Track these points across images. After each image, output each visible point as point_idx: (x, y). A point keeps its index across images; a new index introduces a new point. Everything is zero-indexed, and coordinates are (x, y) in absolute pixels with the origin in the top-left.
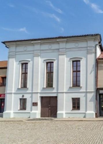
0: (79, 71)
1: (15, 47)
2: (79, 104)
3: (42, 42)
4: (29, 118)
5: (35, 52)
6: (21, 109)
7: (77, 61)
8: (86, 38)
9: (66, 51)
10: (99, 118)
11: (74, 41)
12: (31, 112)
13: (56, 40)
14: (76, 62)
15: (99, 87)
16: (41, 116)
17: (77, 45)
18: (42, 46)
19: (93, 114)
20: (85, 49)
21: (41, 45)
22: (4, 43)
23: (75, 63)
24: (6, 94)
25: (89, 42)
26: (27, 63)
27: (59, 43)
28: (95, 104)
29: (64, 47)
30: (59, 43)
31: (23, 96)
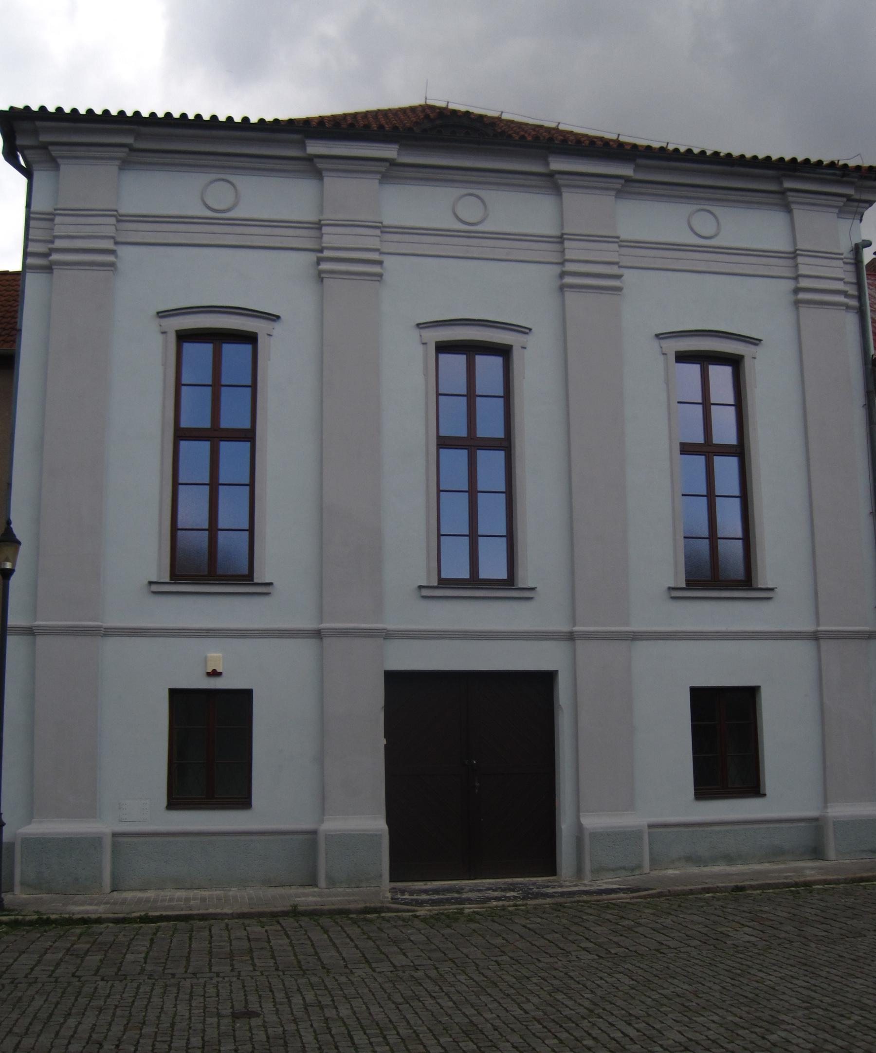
0: (444, 443)
14: (206, 349)
25: (67, 169)
27: (319, 175)
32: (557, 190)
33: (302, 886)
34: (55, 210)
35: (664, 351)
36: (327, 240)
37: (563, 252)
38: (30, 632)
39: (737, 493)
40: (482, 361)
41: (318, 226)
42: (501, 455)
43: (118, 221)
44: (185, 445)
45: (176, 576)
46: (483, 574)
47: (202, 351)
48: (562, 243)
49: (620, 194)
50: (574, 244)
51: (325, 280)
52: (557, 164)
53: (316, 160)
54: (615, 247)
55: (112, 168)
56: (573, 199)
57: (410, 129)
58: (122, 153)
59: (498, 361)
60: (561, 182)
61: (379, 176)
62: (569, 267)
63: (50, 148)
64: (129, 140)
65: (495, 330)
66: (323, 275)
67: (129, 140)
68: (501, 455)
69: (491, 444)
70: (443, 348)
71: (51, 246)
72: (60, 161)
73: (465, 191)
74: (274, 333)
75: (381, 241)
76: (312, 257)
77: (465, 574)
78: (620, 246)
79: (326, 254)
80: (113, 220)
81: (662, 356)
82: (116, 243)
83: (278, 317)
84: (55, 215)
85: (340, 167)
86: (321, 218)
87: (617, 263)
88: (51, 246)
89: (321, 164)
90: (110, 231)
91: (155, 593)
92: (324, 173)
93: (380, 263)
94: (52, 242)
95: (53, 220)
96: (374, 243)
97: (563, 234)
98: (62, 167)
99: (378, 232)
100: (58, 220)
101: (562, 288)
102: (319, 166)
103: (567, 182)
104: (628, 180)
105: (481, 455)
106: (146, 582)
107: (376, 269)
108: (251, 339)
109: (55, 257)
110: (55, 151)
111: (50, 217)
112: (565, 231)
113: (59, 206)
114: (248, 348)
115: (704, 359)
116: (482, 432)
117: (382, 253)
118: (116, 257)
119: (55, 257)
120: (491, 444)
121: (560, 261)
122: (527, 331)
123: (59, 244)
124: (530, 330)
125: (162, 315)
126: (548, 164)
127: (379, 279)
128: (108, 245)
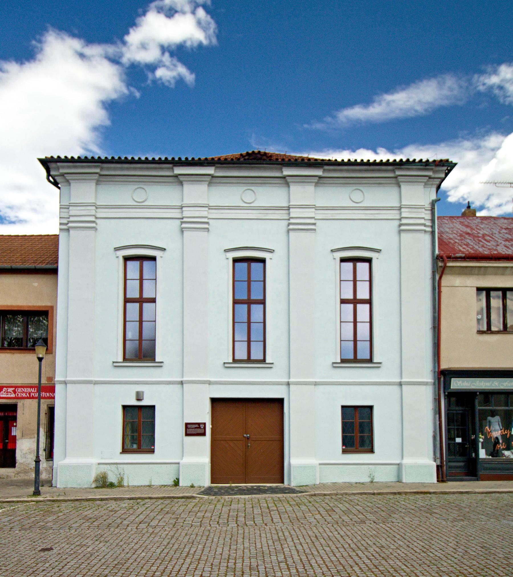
0: (153, 300)
1: (94, 184)
2: (346, 427)
3: (326, 175)
4: (176, 483)
5: (72, 213)
6: (125, 451)
7: (141, 258)
8: (398, 173)
9: (96, 218)
10: (450, 483)
11: (346, 181)
12: (181, 462)
13: (172, 169)
14: (137, 264)
15: (444, 366)
16: (213, 480)
17: (357, 196)
18: (99, 187)
19: (203, 465)
20: (283, 214)
21: (98, 182)
22: (46, 163)
23: (133, 267)
24: (58, 388)
25: (405, 188)
26: (153, 259)
27: (181, 183)
28: (435, 432)
29: (91, 200)
30: (181, 183)
31: (139, 397)
32: (288, 185)
33: (320, 477)
34: (70, 203)
35: (335, 257)
36: (186, 214)
37: (289, 214)
38: (65, 383)
39: (352, 321)
40: (359, 265)
41: (289, 208)
42: (368, 306)
43: (97, 208)
44: (129, 305)
45: (125, 359)
46: (359, 357)
47: (244, 265)
48: (289, 210)
49: (317, 184)
50: (406, 210)
51: (184, 232)
52: (287, 172)
53: (287, 178)
54: (313, 210)
55: (92, 185)
56: (295, 189)
57: (239, 159)
58: (96, 177)
59: (367, 265)
60: (289, 180)
61: (423, 184)
62: (292, 221)
63: (65, 175)
64: (98, 170)
65: (258, 251)
66: (183, 230)
67: (98, 170)
68: (368, 306)
69: (363, 302)
70: (343, 260)
71: (68, 220)
72: (70, 181)
73: (355, 188)
74: (379, 257)
75: (208, 213)
76: (178, 222)
77: (245, 357)
78: (316, 209)
79: (185, 220)
80: (94, 208)
81: (226, 260)
82: (96, 218)
83: (165, 249)
84: (70, 206)
85: (189, 179)
86: (182, 203)
87: (423, 218)
88: (68, 220)
89: (289, 179)
90: (93, 213)
91: (116, 366)
92: (184, 183)
93: (314, 224)
94: (69, 218)
95: (68, 208)
96: (205, 214)
97: (289, 205)
98: (72, 184)
99: (207, 209)
100: (71, 208)
101: (400, 232)
102: (68, 178)
103: (292, 180)
104: (320, 177)
105: (359, 306)
106: (331, 363)
107: (206, 226)
108: (263, 261)
109: (70, 225)
110: (289, 179)
111: (67, 207)
112: (291, 204)
113: (71, 202)
114: (261, 265)
115: (355, 260)
116: (359, 296)
117: (209, 219)
118: (97, 224)
119: (70, 225)
120: (363, 302)
121: (288, 218)
122: (272, 251)
123: (72, 219)
124: (274, 251)
125: (117, 249)
126: (282, 172)
127: (207, 230)
128: (92, 219)
